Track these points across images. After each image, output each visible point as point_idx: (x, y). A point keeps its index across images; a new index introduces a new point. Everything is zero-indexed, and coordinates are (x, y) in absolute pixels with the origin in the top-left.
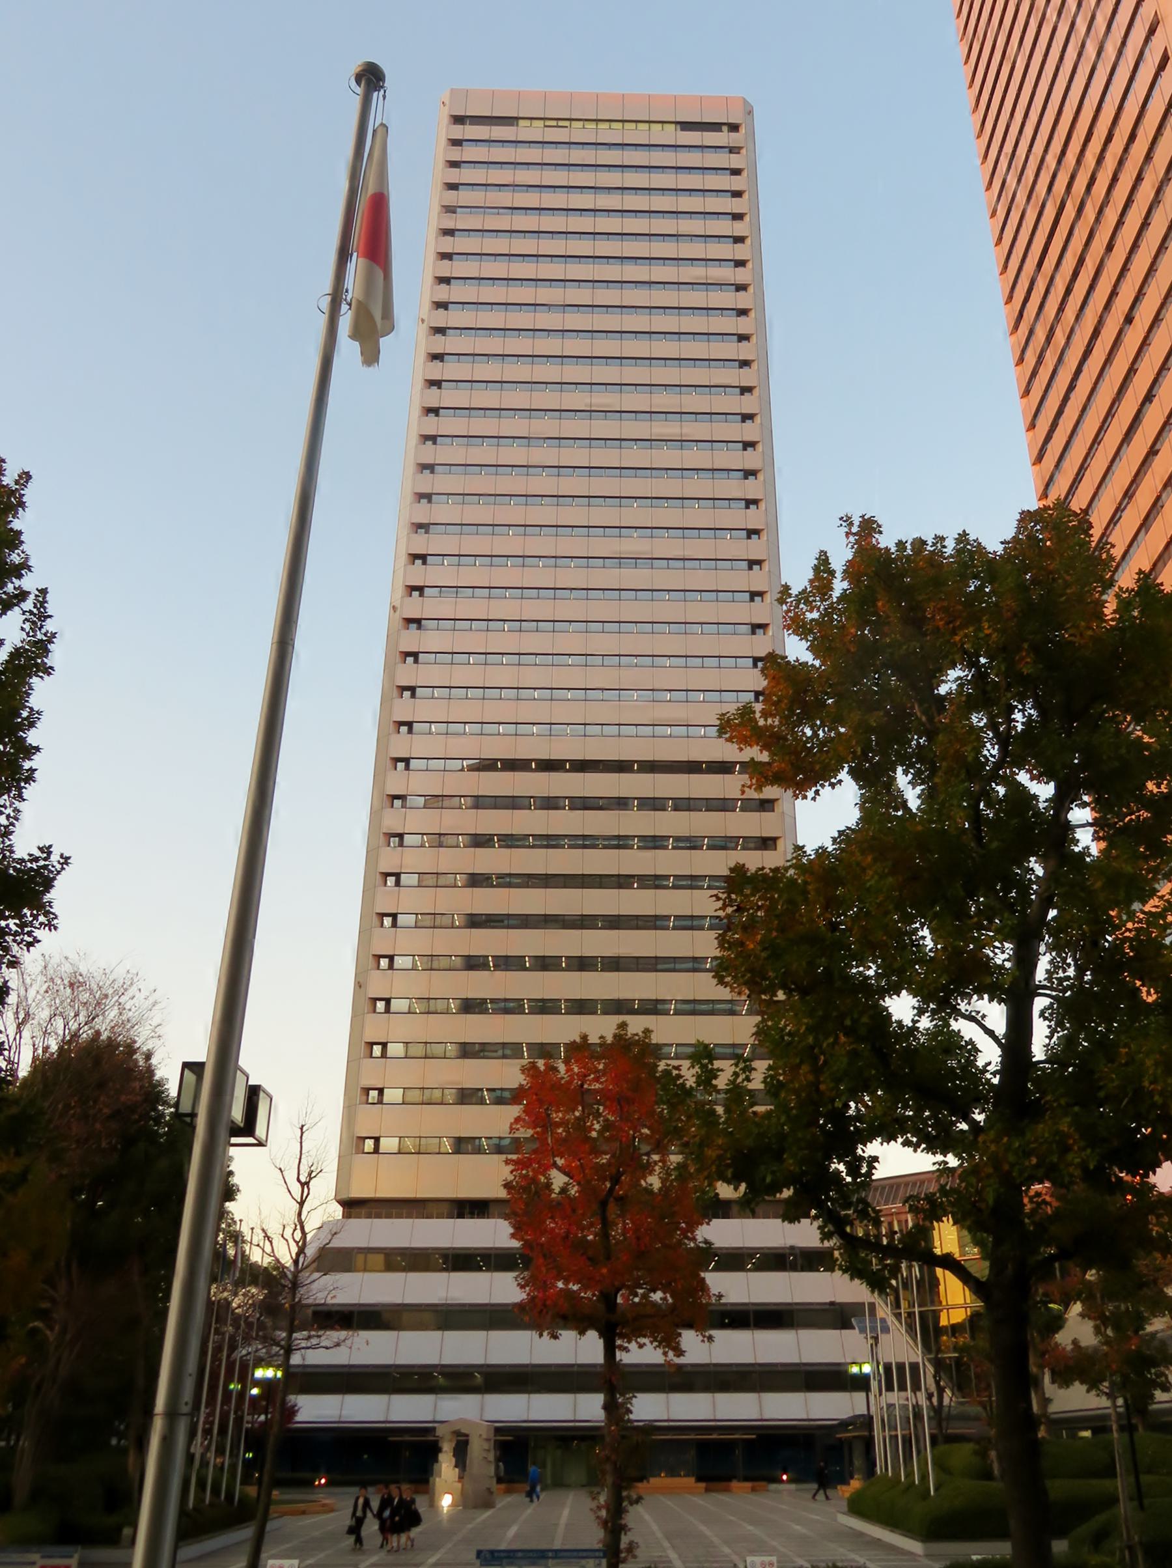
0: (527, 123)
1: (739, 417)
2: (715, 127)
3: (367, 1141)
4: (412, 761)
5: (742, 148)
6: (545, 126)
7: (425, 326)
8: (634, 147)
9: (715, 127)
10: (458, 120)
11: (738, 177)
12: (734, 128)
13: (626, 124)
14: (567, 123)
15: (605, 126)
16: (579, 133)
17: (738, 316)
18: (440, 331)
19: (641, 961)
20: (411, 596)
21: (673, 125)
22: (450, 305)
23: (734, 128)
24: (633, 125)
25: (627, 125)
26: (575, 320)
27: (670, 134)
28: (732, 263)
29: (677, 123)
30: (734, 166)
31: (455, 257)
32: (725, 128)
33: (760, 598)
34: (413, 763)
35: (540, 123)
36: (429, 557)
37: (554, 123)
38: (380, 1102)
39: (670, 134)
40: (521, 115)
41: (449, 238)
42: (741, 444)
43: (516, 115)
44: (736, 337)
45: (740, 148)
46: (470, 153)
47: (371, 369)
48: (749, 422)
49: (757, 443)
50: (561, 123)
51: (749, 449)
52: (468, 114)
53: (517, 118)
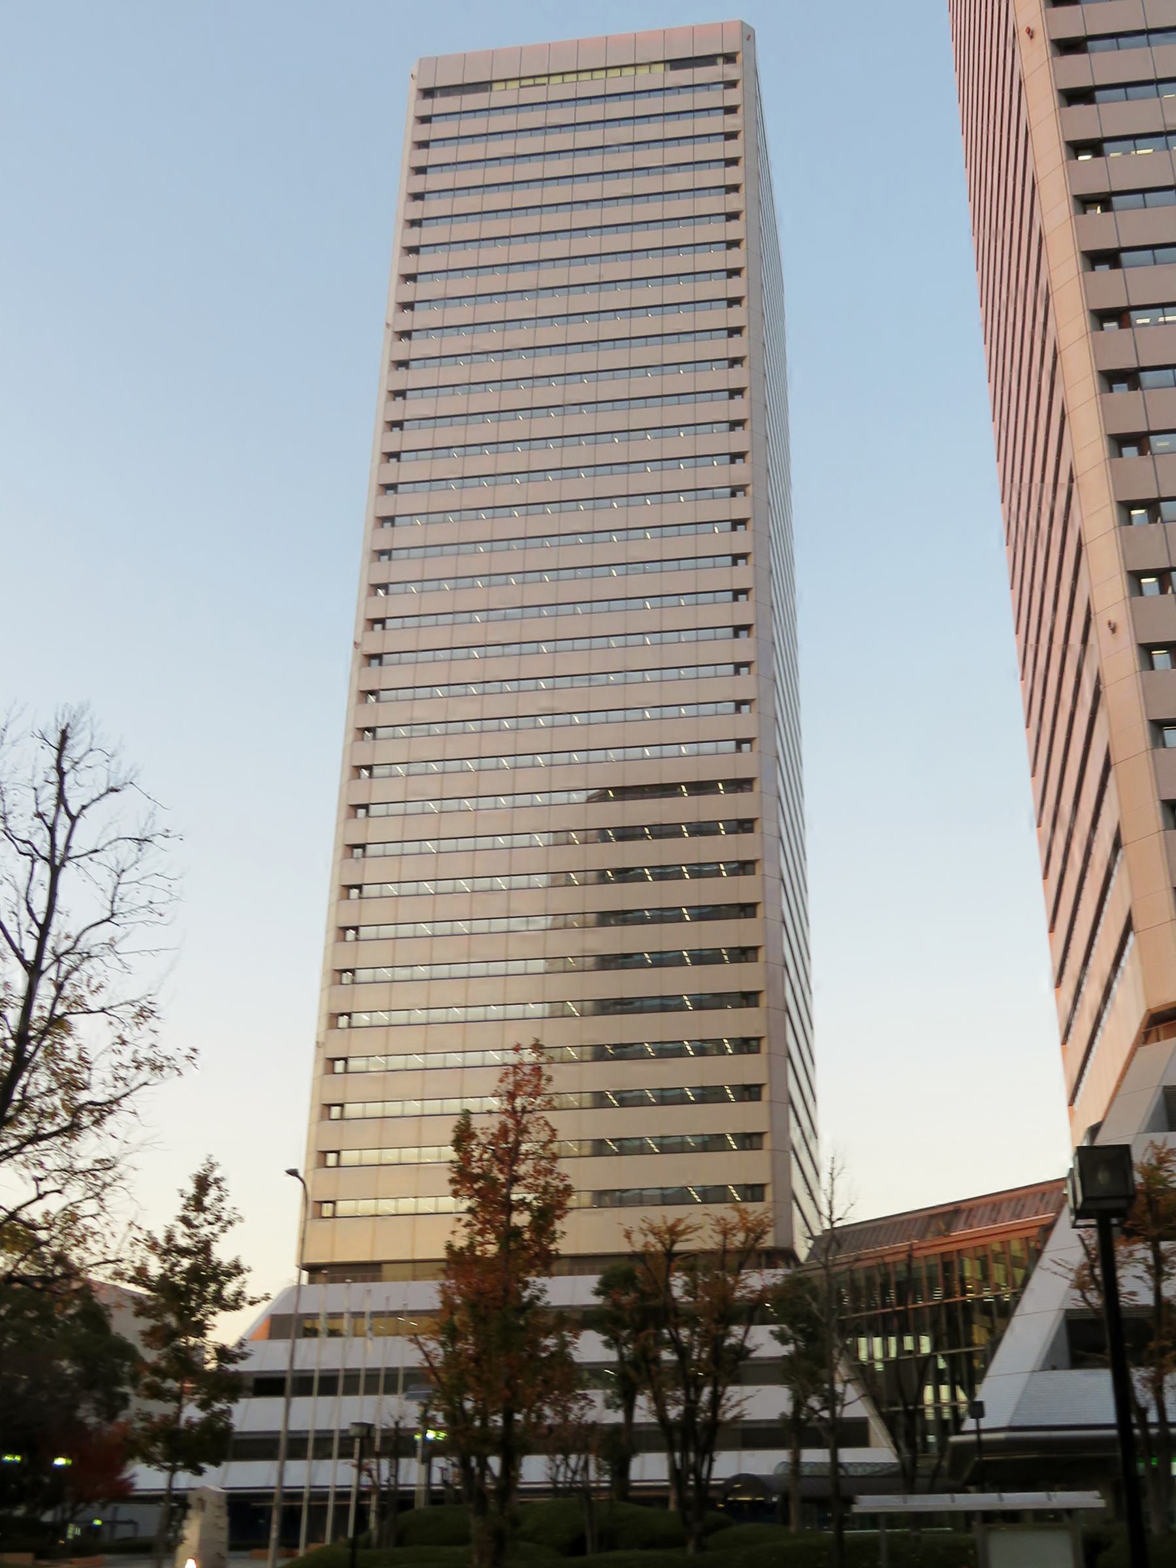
0: (501, 86)
1: (725, 332)
2: (708, 60)
3: (325, 1205)
4: (372, 807)
5: (747, 485)
6: (521, 87)
7: (390, 332)
8: (617, 98)
9: (708, 60)
10: (428, 93)
11: (734, 89)
12: (730, 58)
13: (609, 71)
14: (545, 80)
15: (587, 76)
16: (558, 89)
17: (727, 193)
18: (406, 334)
19: (606, 1003)
20: (373, 629)
21: (662, 66)
22: (416, 305)
23: (730, 58)
24: (617, 72)
25: (611, 73)
26: (547, 364)
27: (659, 76)
28: (722, 137)
29: (665, 62)
30: (728, 103)
31: (422, 249)
32: (720, 61)
33: (744, 561)
34: (376, 771)
35: (515, 84)
36: (391, 586)
37: (531, 82)
38: (342, 1118)
39: (659, 76)
40: (494, 78)
41: (416, 229)
42: (728, 457)
43: (489, 79)
44: (724, 245)
45: (755, 949)
46: (439, 129)
47: (138, 1319)
48: (736, 336)
49: (746, 453)
50: (538, 81)
51: (736, 397)
52: (438, 84)
53: (491, 82)
